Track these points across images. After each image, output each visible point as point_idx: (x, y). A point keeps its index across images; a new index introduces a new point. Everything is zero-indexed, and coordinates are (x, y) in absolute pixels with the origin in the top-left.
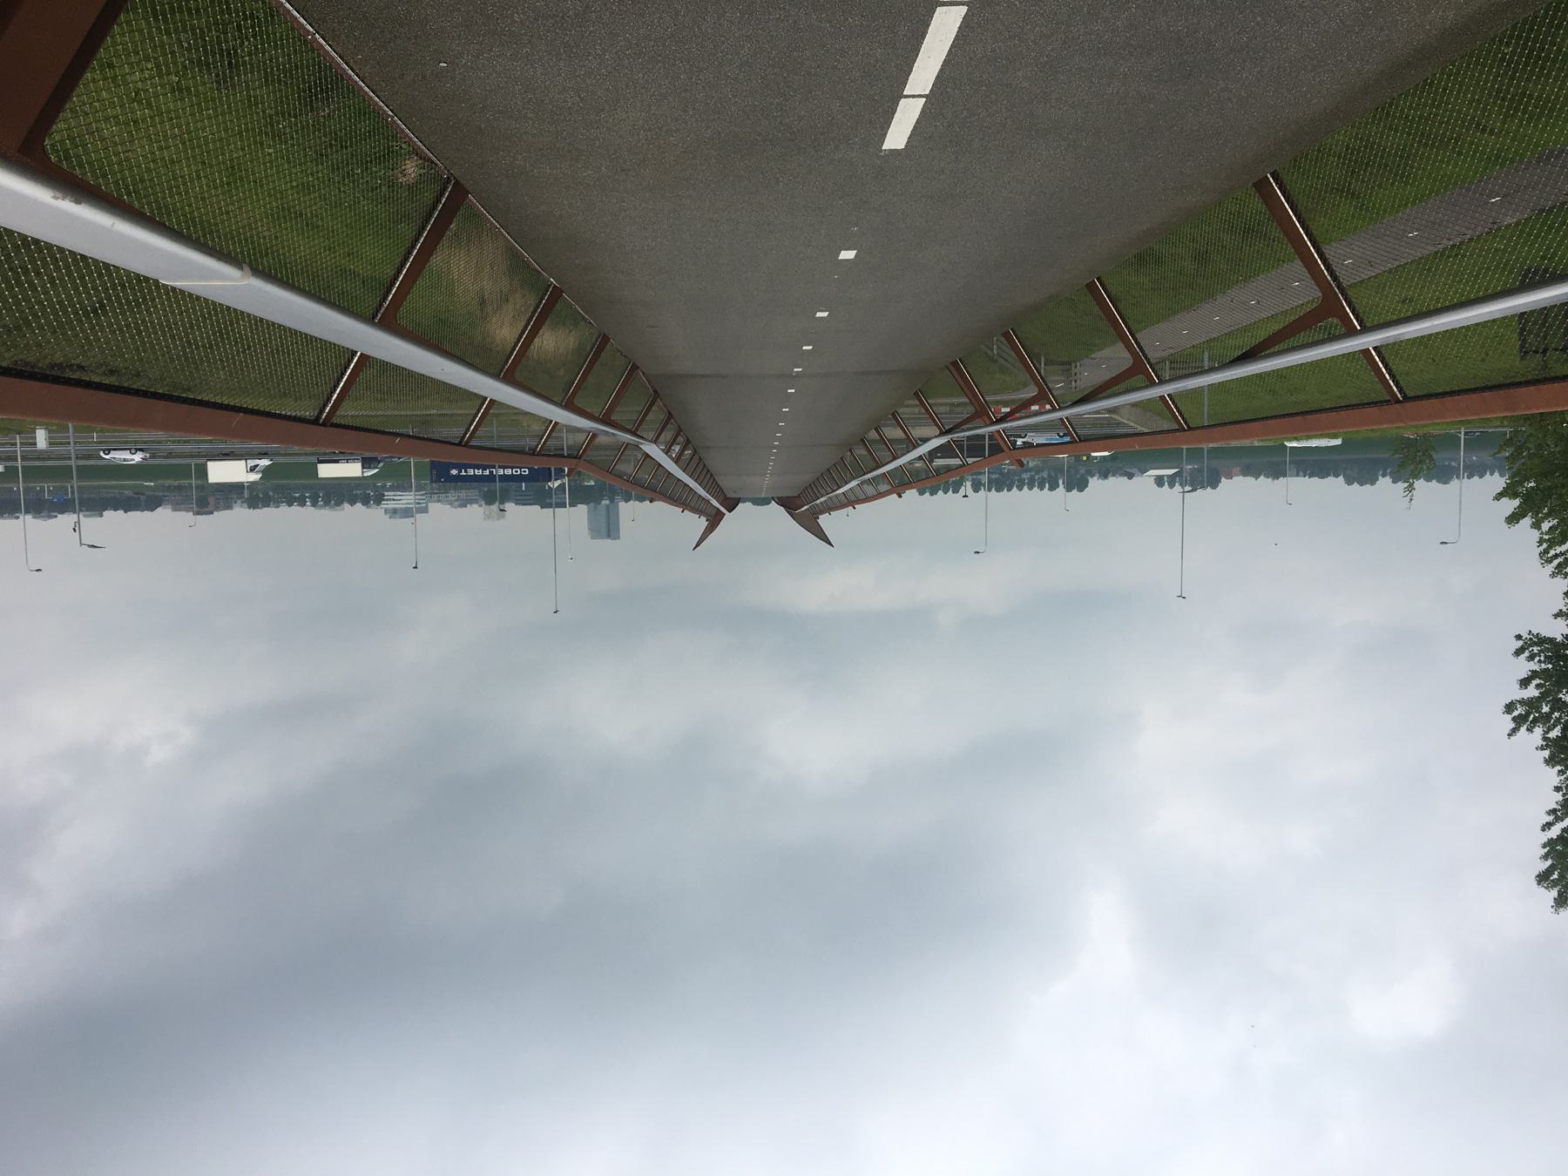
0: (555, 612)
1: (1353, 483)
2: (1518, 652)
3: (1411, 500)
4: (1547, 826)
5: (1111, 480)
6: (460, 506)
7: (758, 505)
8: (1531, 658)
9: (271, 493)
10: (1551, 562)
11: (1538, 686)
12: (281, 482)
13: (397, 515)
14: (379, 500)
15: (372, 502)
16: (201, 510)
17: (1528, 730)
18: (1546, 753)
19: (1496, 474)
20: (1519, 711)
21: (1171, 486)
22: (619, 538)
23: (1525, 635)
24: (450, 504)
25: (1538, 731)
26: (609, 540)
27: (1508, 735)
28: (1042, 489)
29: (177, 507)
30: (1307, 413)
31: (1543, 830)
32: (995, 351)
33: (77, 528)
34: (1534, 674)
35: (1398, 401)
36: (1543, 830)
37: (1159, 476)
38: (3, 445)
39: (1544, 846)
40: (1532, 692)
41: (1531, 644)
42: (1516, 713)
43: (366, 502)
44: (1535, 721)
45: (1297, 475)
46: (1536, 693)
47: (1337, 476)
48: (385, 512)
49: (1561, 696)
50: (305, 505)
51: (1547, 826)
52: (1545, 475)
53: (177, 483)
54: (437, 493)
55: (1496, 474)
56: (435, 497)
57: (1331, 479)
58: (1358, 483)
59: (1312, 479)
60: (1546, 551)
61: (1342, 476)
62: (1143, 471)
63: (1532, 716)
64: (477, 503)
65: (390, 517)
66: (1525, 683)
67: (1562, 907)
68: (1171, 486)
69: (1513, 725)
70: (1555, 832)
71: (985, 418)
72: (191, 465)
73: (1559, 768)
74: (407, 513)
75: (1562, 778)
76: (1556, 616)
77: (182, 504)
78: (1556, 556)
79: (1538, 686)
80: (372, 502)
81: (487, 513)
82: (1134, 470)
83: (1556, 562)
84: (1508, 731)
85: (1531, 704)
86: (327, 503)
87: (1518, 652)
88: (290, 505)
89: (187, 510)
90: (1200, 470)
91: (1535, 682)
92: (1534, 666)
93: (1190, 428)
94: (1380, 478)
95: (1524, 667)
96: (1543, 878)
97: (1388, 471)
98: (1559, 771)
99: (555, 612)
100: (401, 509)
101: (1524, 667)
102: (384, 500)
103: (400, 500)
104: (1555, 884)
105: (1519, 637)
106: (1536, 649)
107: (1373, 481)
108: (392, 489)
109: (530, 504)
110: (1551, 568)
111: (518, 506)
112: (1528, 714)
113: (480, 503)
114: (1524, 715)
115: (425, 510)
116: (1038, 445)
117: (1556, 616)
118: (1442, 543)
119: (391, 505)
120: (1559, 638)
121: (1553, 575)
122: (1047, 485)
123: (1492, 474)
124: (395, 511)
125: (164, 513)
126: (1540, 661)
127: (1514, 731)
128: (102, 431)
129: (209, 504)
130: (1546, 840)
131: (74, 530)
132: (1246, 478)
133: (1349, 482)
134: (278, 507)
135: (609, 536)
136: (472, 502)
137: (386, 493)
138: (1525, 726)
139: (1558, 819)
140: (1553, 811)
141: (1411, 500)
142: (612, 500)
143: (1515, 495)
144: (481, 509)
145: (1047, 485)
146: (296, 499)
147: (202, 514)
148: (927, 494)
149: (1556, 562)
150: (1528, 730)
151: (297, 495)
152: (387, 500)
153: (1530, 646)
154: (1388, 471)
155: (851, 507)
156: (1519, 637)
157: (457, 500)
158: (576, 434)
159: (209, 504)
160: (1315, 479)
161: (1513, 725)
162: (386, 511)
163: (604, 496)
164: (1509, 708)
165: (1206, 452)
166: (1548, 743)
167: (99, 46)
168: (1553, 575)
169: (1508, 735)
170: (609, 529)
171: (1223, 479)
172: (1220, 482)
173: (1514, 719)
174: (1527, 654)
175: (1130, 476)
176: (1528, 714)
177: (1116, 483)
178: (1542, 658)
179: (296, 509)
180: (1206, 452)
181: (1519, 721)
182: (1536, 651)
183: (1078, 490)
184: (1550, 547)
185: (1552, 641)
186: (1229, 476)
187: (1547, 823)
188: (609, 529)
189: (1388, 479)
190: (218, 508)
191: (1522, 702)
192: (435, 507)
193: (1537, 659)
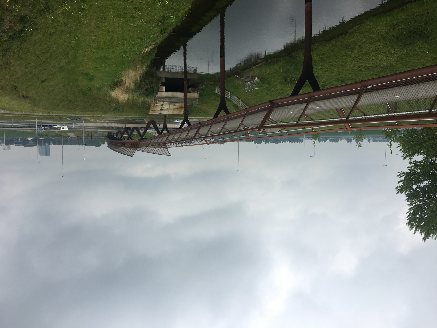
4: (408, 212)
7: (97, 146)
20: (399, 188)
22: (49, 156)
26: (46, 156)
30: (377, 126)
32: (241, 105)
34: (401, 181)
38: (1, 123)
61: (106, 143)
66: (399, 182)
81: (4, 148)
84: (397, 193)
94: (262, 142)
98: (407, 201)
99: (63, 177)
101: (399, 179)
105: (399, 172)
107: (261, 143)
111: (16, 146)
116: (322, 131)
118: (310, 156)
123: (322, 142)
127: (398, 193)
135: (46, 155)
142: (49, 144)
144: (2, 146)
148: (294, 142)
154: (264, 141)
158: (104, 124)
160: (248, 142)
164: (397, 188)
165: (62, 132)
166: (407, 195)
167: (313, 69)
170: (47, 153)
174: (400, 176)
180: (62, 132)
188: (47, 153)
189: (264, 143)
191: (400, 187)
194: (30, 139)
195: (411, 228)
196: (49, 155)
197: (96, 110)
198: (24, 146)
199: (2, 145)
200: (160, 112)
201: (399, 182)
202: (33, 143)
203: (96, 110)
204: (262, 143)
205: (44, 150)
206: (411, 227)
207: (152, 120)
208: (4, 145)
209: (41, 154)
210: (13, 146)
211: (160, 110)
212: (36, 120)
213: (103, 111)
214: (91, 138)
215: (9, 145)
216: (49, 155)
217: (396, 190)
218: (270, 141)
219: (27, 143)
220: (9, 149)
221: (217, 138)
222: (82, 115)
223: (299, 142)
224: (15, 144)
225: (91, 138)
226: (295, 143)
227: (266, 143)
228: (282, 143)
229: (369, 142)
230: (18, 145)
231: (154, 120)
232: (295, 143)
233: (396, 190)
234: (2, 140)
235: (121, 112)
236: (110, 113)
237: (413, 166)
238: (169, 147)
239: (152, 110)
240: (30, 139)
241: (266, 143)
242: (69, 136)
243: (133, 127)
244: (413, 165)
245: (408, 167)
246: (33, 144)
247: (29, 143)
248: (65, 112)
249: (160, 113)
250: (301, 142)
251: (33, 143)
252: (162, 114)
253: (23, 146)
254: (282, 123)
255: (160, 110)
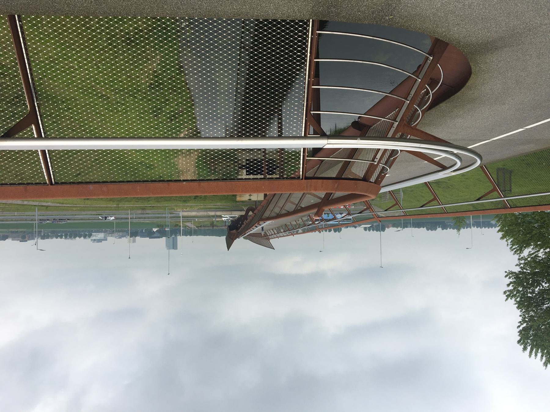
0: (169, 274)
1: (482, 228)
2: (506, 276)
3: (459, 234)
4: (519, 326)
5: (349, 228)
6: (119, 238)
8: (510, 278)
9: (50, 234)
10: (513, 251)
11: (512, 286)
12: (61, 230)
13: (96, 242)
14: (90, 236)
15: (87, 237)
16: (23, 240)
17: (511, 299)
18: (517, 305)
19: (475, 227)
20: (508, 293)
21: (369, 230)
22: (177, 249)
23: (508, 271)
24: (116, 237)
25: (513, 299)
26: (174, 250)
27: (505, 301)
28: (326, 231)
29: (14, 238)
31: (518, 328)
33: (36, 244)
34: (511, 283)
35: (508, 208)
36: (518, 328)
37: (365, 227)
38: (1, 216)
39: (518, 332)
40: (511, 288)
41: (510, 274)
42: (507, 294)
43: (85, 237)
44: (512, 296)
45: (411, 227)
46: (512, 288)
47: (423, 227)
48: (91, 240)
49: (519, 288)
50: (62, 238)
51: (519, 326)
52: (510, 225)
53: (16, 230)
54: (111, 233)
55: (475, 227)
56: (110, 235)
57: (422, 228)
58: (431, 230)
59: (416, 228)
60: (511, 247)
62: (360, 226)
63: (511, 295)
64: (125, 237)
65: (93, 242)
66: (508, 285)
67: (525, 351)
68: (369, 230)
69: (506, 298)
70: (521, 328)
71: (370, 209)
72: (34, 223)
73: (520, 310)
74: (100, 241)
75: (522, 312)
76: (516, 265)
77: (16, 238)
78: (514, 249)
79: (512, 286)
80: (87, 237)
82: (357, 225)
83: (514, 250)
84: (505, 299)
85: (510, 291)
86: (71, 237)
87: (506, 276)
88: (57, 238)
89: (17, 240)
90: (379, 225)
91: (511, 285)
92: (511, 280)
93: (448, 213)
94: (438, 228)
95: (508, 281)
96: (519, 342)
97: (440, 226)
99: (169, 274)
100: (97, 239)
101: (508, 281)
102: (92, 236)
103: (98, 236)
104: (522, 344)
105: (506, 272)
106: (511, 275)
107: (435, 229)
108: (96, 232)
109: (145, 237)
110: (513, 252)
112: (510, 294)
113: (126, 237)
114: (509, 295)
115: (106, 240)
117: (516, 265)
118: (467, 248)
119: (94, 238)
120: (517, 272)
121: (514, 254)
122: (328, 230)
124: (95, 240)
125: (9, 241)
126: (513, 279)
127: (507, 299)
128: (17, 212)
129: (26, 238)
130: (519, 330)
131: (35, 244)
132: (221, 237)
133: (428, 229)
134: (52, 239)
135: (173, 248)
136: (123, 236)
137: (93, 234)
138: (510, 298)
139: (522, 324)
140: (520, 322)
141: (459, 234)
142: (176, 236)
143: (503, 231)
145: (328, 230)
146: (59, 236)
147: (23, 242)
149: (514, 250)
150: (511, 299)
151: (60, 234)
152: (93, 236)
153: (509, 274)
154: (440, 226)
155: (292, 236)
156: (506, 272)
157: (118, 236)
159: (26, 238)
160: (417, 229)
161: (506, 298)
162: (92, 240)
163: (173, 234)
164: (505, 292)
168: (514, 254)
169: (505, 301)
170: (174, 246)
171: (386, 228)
172: (385, 229)
173: (506, 296)
174: (508, 277)
175: (355, 227)
176: (510, 294)
177: (351, 230)
178: (513, 278)
179: (59, 239)
181: (508, 296)
182: (511, 276)
183: (338, 232)
184: (513, 246)
185: (515, 273)
186: (388, 227)
187: (519, 326)
189: (440, 229)
190: (29, 239)
192: (109, 238)
193: (511, 278)
194: (155, 230)
195: (525, 349)
196: (177, 249)
197: (174, 200)
198: (150, 238)
199: (127, 238)
200: (249, 198)
201: (508, 285)
202: (159, 235)
203: (174, 200)
204: (437, 229)
205: (172, 242)
206: (524, 347)
207: (251, 207)
208: (129, 237)
209: (168, 247)
210: (138, 238)
211: (249, 195)
212: (129, 210)
213: (182, 200)
214: (213, 228)
215: (134, 237)
216: (177, 249)
217: (505, 295)
218: (449, 227)
219: (153, 235)
220: (134, 241)
221: (375, 223)
222: (143, 205)
223: (492, 228)
224: (140, 236)
225: (213, 228)
226: (485, 228)
227: (443, 229)
228: (467, 228)
229: (335, 232)
230: (143, 237)
231: (253, 207)
232: (485, 228)
233: (505, 295)
234: (127, 232)
235: (179, 201)
236: (191, 201)
237: (522, 264)
238: (271, 239)
239: (240, 196)
240: (155, 230)
241: (443, 229)
242: (188, 226)
243: (241, 215)
244: (523, 262)
245: (516, 264)
246: (159, 236)
247: (155, 234)
248: (137, 203)
249: (250, 199)
250: (494, 228)
251: (159, 234)
252: (252, 200)
253: (148, 238)
254: (442, 205)
255: (248, 196)
